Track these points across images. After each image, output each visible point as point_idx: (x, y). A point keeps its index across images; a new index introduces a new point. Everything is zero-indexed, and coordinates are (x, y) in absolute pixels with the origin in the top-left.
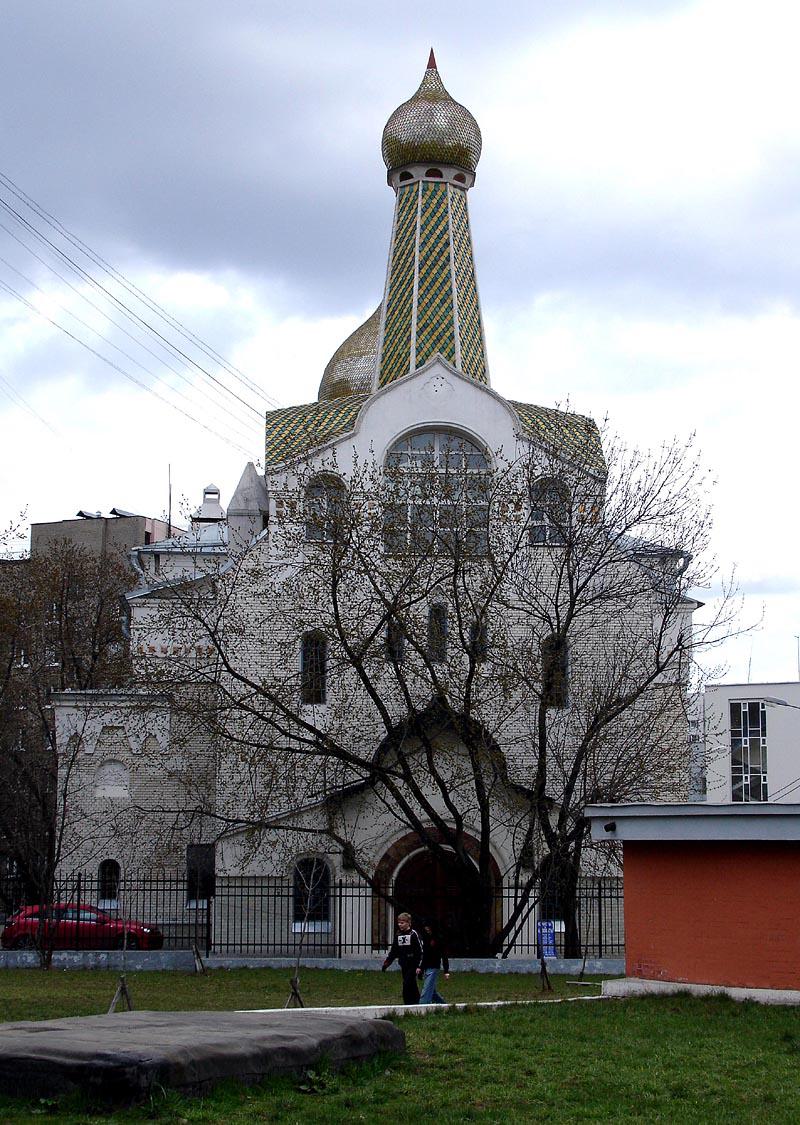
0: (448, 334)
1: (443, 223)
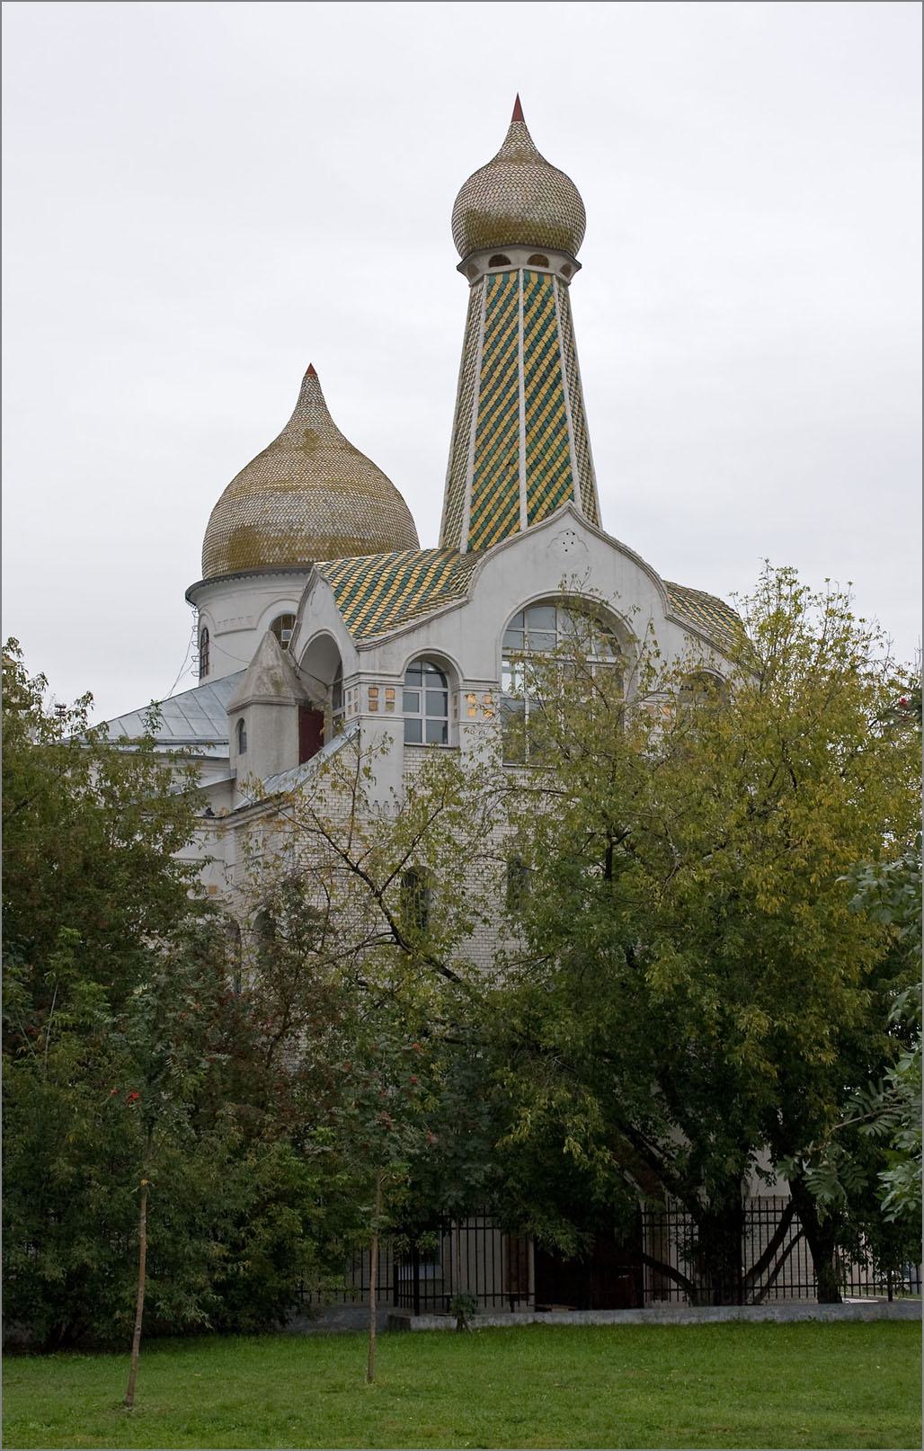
0: (564, 475)
1: (551, 328)
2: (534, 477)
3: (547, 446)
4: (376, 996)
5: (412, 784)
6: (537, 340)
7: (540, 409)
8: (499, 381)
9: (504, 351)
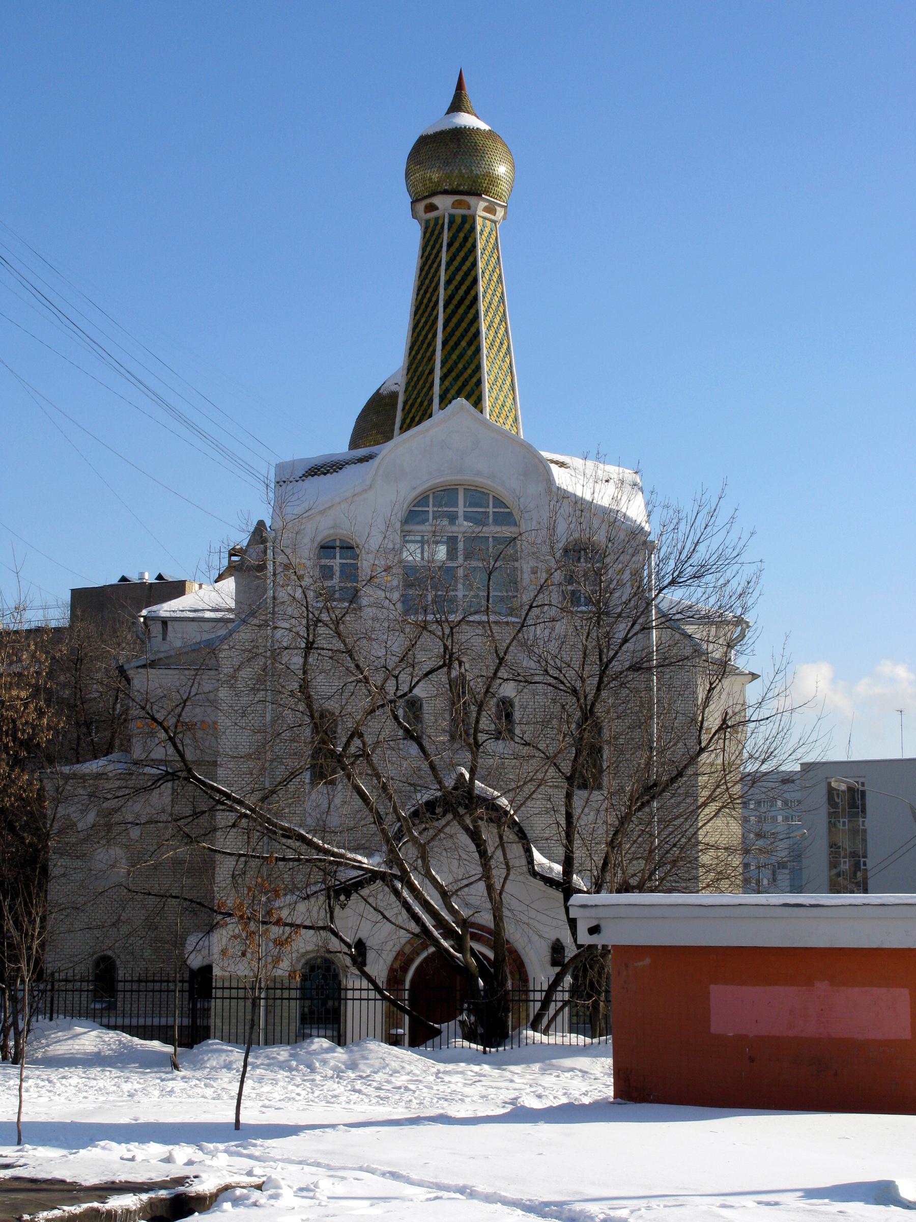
2: (447, 383)
3: (460, 357)
4: (285, 588)
5: (414, 1101)
6: (458, 269)
7: (457, 326)
8: (427, 306)
9: (431, 282)
